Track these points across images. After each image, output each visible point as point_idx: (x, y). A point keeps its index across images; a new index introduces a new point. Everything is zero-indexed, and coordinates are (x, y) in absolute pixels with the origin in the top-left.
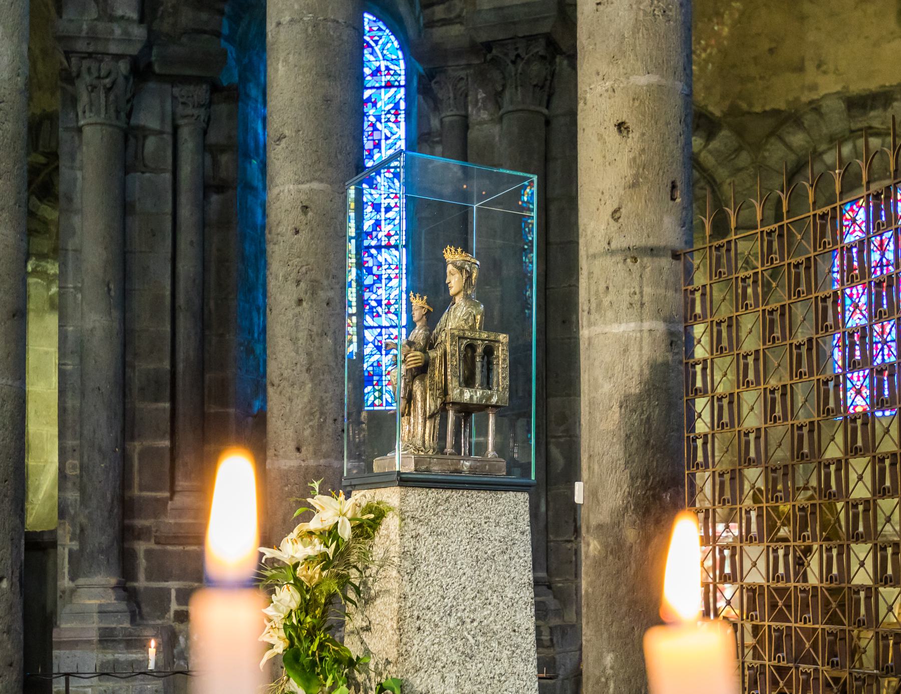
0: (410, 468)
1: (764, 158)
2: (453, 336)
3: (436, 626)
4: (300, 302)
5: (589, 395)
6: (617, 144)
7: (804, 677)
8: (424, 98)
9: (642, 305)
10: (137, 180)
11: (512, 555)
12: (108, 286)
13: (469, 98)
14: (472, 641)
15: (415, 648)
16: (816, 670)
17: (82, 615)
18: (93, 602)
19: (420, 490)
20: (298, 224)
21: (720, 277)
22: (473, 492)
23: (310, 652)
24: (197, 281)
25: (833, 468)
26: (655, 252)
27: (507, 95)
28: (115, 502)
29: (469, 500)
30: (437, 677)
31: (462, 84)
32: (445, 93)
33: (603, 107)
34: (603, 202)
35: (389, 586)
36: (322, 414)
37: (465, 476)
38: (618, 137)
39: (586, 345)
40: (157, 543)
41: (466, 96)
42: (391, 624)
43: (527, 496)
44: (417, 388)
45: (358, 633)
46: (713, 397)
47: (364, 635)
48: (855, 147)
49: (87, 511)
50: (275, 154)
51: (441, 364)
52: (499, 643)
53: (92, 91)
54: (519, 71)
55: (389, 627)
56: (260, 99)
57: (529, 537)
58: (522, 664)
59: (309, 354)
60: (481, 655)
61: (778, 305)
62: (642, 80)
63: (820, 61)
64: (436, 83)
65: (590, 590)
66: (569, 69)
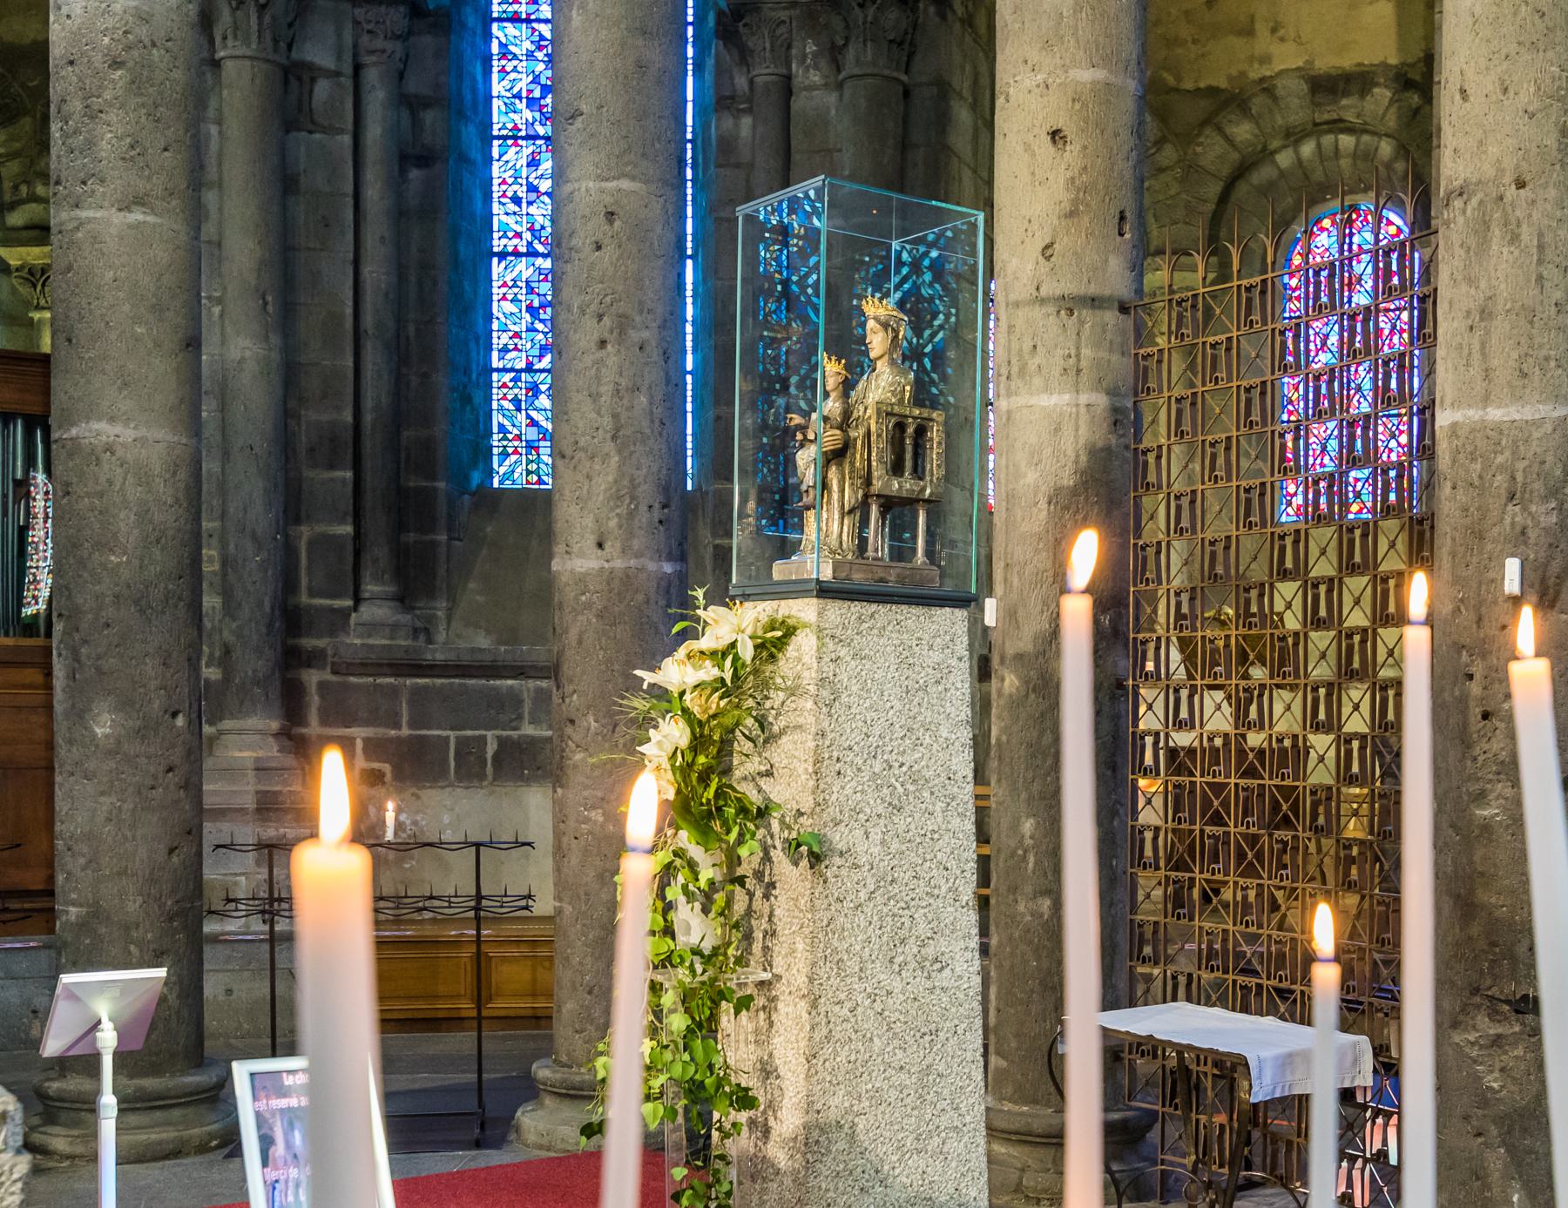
0: (827, 573)
1: (1195, 154)
2: (879, 412)
3: (859, 770)
4: (603, 343)
5: (1006, 485)
6: (1050, 161)
7: (1280, 846)
8: (725, 45)
9: (1079, 371)
10: (303, 144)
11: (948, 686)
12: (264, 299)
13: (794, 51)
14: (900, 790)
15: (834, 797)
16: (1295, 838)
17: (231, 772)
18: (246, 754)
19: (841, 602)
20: (601, 236)
21: (1182, 340)
22: (903, 607)
23: (704, 801)
24: (391, 296)
25: (1323, 589)
26: (1097, 303)
27: (851, 54)
28: (277, 613)
29: (898, 617)
30: (859, 833)
31: (782, 30)
32: (759, 42)
33: (1033, 107)
34: (1030, 234)
35: (801, 720)
36: (633, 498)
37: (892, 585)
38: (1052, 149)
39: (1004, 420)
40: (334, 672)
41: (789, 47)
42: (804, 768)
43: (966, 613)
44: (833, 475)
45: (753, 780)
46: (1169, 494)
47: (762, 782)
48: (1319, 145)
49: (234, 625)
50: (567, 137)
51: (863, 442)
52: (932, 793)
53: (237, 8)
54: (869, 18)
55: (801, 771)
56: (479, 31)
57: (967, 664)
58: (959, 820)
59: (615, 416)
60: (911, 808)
61: (1258, 380)
62: (1086, 75)
63: (1276, 22)
64: (745, 25)
65: (1004, 738)
66: (937, 19)
